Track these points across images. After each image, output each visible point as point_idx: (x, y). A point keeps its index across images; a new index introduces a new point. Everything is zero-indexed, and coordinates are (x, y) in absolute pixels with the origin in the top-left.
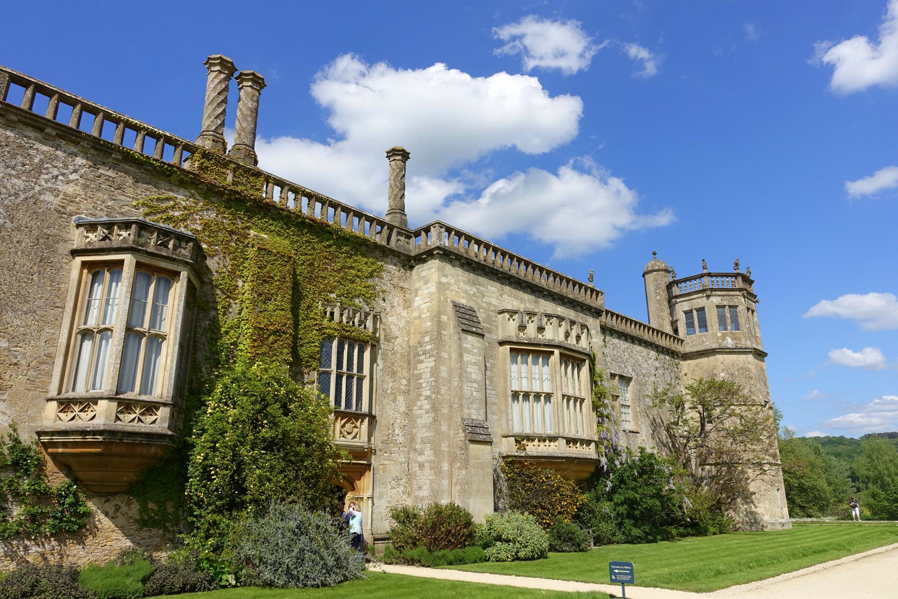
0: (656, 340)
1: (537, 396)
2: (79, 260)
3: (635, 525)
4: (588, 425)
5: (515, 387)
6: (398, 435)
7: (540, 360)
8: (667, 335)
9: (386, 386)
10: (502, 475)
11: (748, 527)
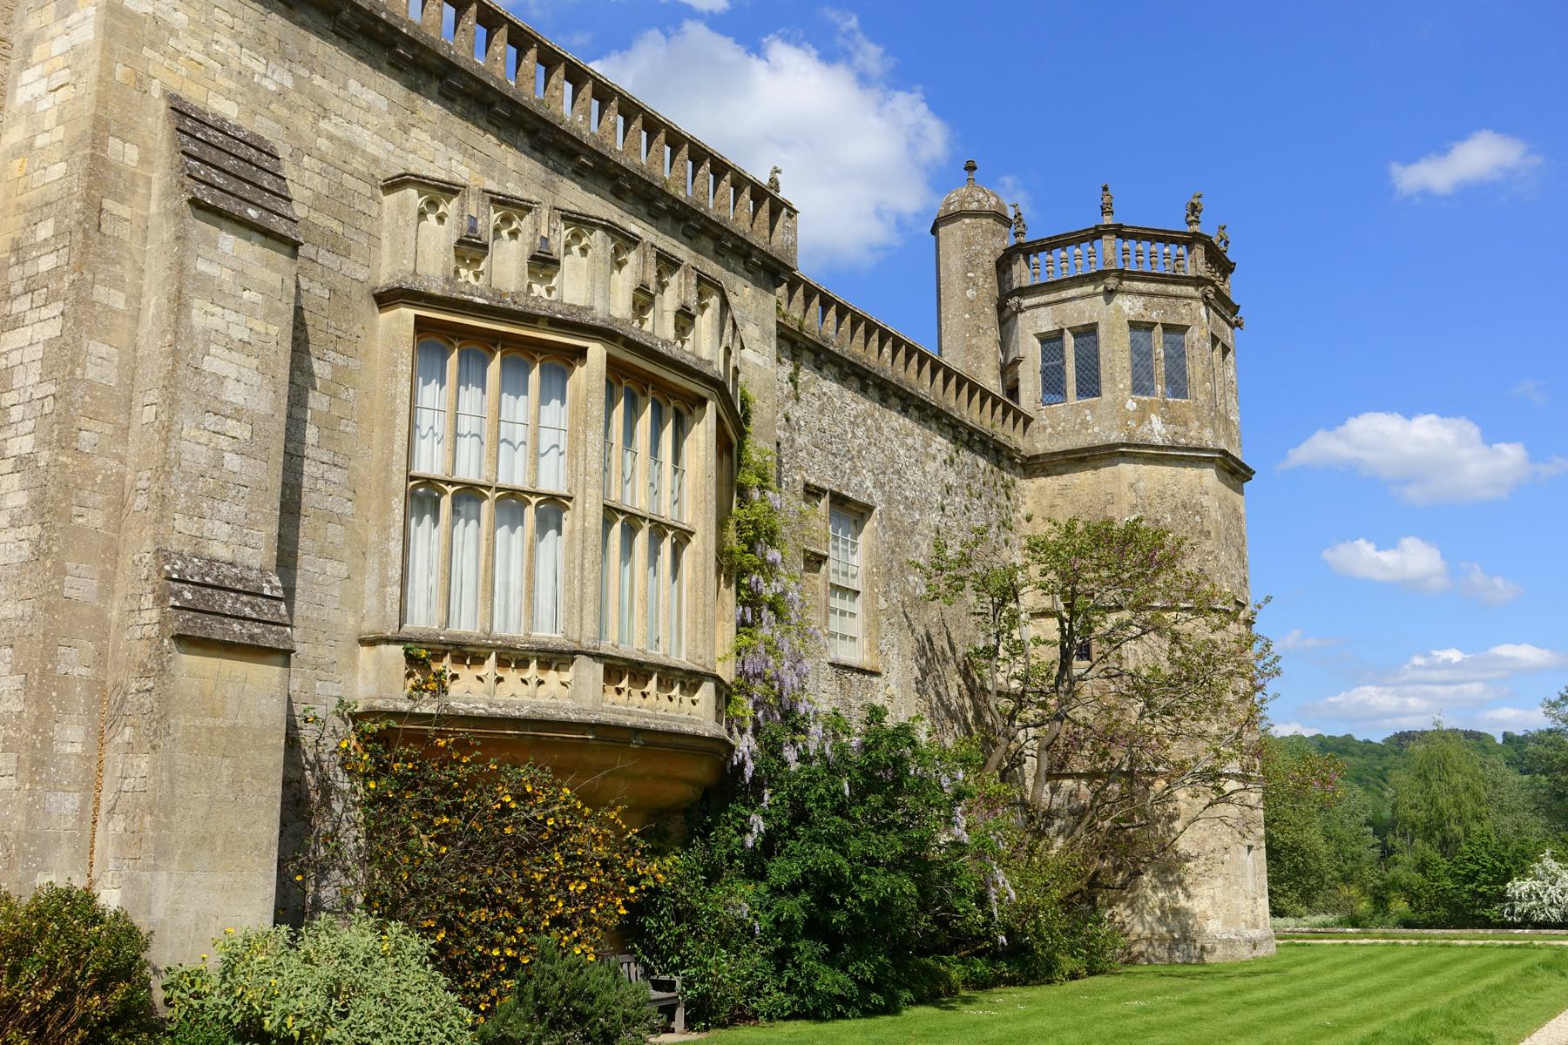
0: (952, 403)
1: (512, 500)
3: (829, 959)
4: (695, 623)
5: (430, 462)
7: (535, 376)
8: (985, 394)
10: (343, 782)
11: (1162, 952)
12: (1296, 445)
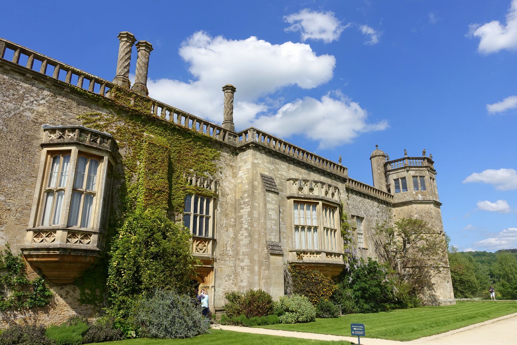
0: (378, 196)
1: (309, 228)
2: (45, 150)
3: (366, 303)
5: (297, 223)
6: (229, 251)
7: (311, 207)
8: (384, 193)
9: (222, 222)
10: (289, 274)
11: (430, 304)
12: (468, 176)
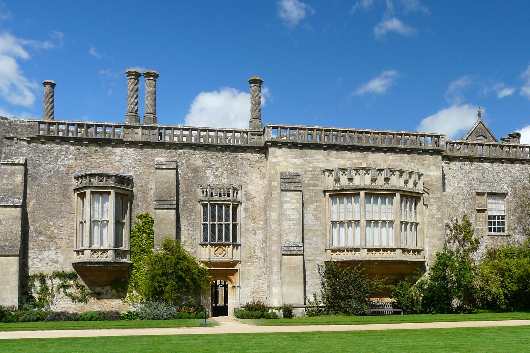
5: (335, 219)
6: (258, 253)
